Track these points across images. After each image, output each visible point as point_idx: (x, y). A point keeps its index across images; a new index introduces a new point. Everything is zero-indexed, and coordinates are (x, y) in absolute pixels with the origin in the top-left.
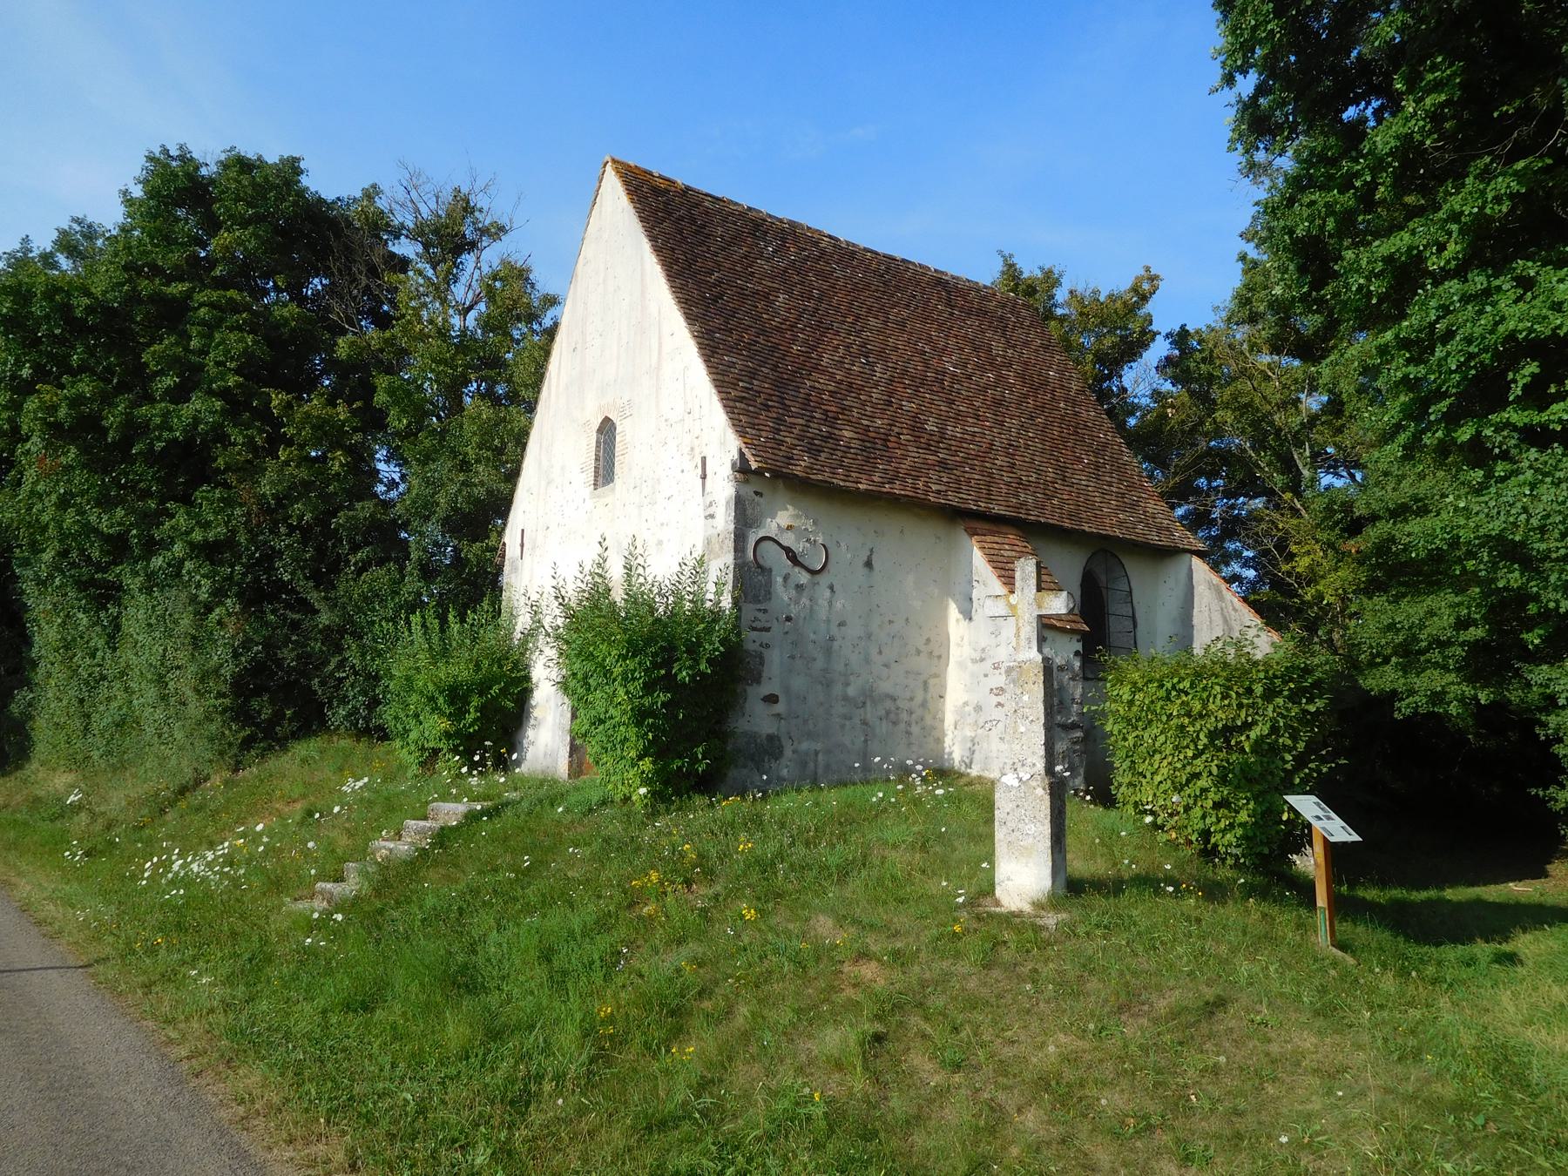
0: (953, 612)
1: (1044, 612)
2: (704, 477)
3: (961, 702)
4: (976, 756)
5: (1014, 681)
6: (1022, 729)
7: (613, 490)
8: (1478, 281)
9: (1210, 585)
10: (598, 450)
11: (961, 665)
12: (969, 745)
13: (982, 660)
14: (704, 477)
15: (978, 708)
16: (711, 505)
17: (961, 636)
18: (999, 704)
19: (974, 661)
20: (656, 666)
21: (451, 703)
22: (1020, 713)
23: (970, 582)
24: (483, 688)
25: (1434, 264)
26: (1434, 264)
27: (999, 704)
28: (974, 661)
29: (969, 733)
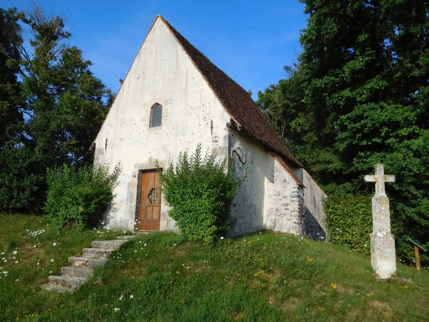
0: (266, 180)
1: (387, 181)
2: (212, 128)
3: (270, 208)
4: (276, 226)
5: (379, 203)
6: (382, 218)
7: (161, 129)
8: (373, 105)
9: (307, 177)
10: (151, 114)
11: (270, 196)
12: (274, 222)
13: (279, 195)
14: (212, 128)
15: (277, 210)
16: (216, 137)
17: (269, 188)
18: (286, 209)
19: (275, 195)
20: (221, 192)
21: (85, 201)
22: (381, 213)
23: (273, 171)
24: (97, 196)
25: (359, 99)
26: (359, 99)
27: (286, 209)
28: (275, 195)
29: (273, 217)
